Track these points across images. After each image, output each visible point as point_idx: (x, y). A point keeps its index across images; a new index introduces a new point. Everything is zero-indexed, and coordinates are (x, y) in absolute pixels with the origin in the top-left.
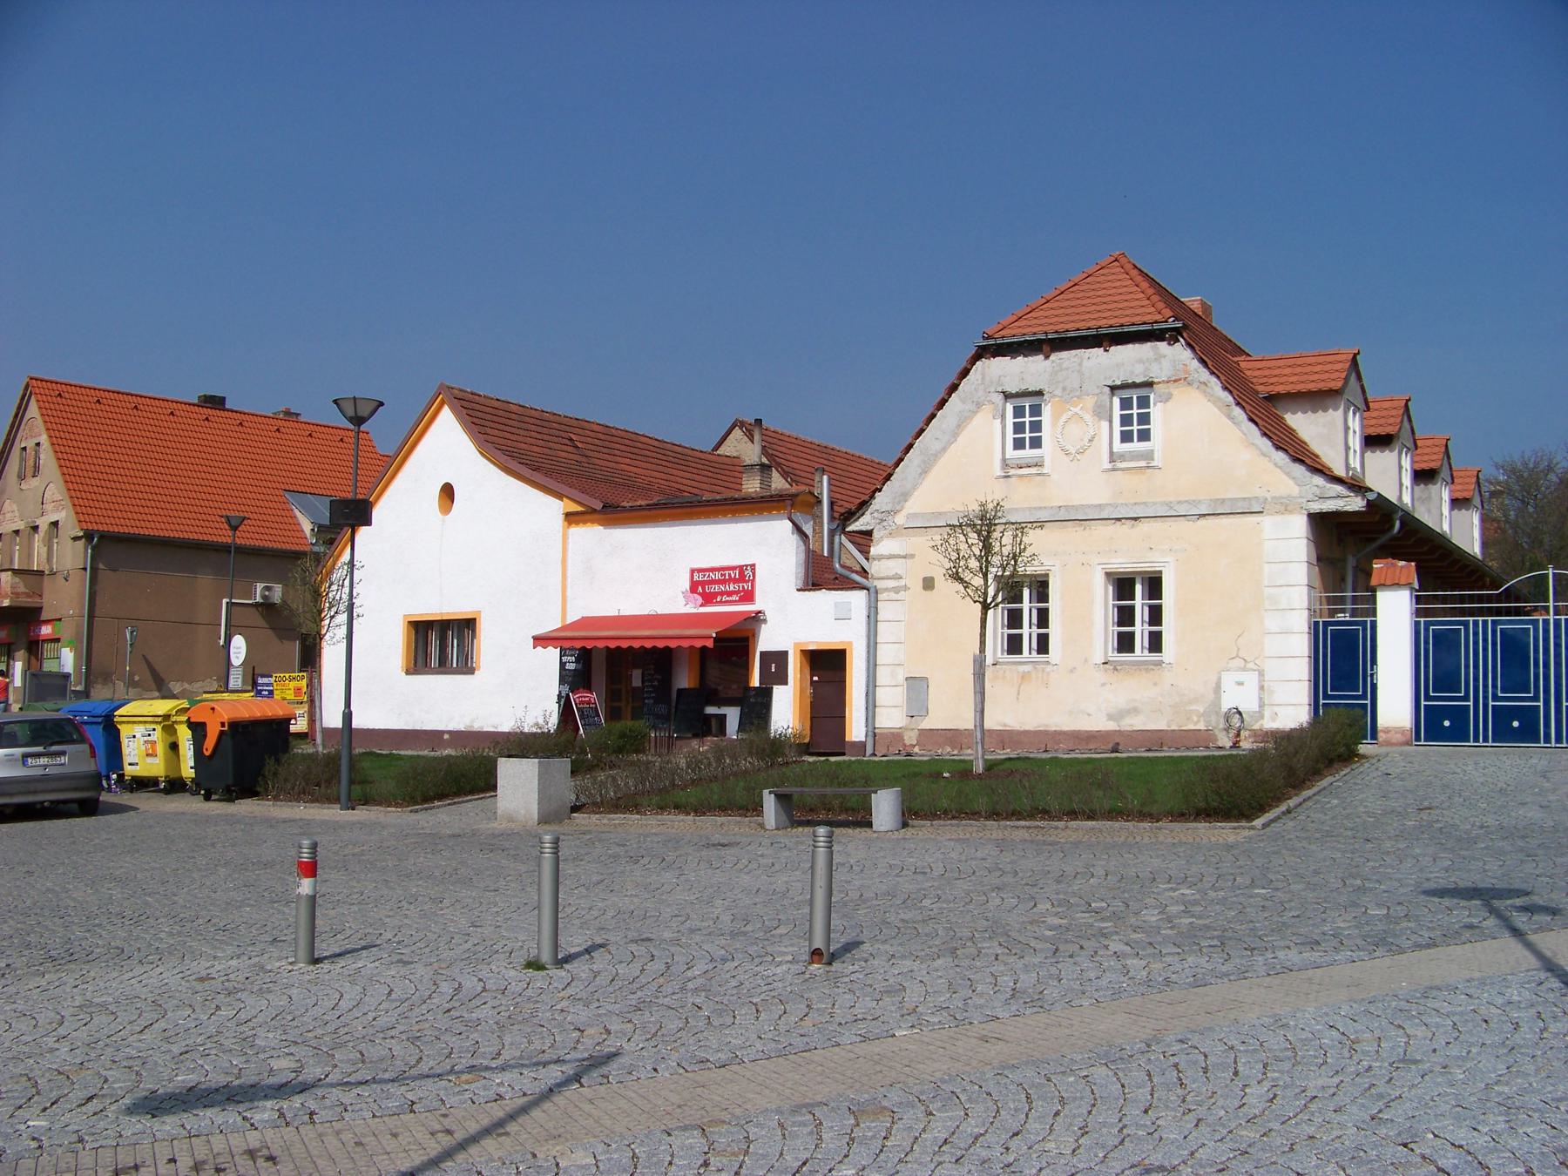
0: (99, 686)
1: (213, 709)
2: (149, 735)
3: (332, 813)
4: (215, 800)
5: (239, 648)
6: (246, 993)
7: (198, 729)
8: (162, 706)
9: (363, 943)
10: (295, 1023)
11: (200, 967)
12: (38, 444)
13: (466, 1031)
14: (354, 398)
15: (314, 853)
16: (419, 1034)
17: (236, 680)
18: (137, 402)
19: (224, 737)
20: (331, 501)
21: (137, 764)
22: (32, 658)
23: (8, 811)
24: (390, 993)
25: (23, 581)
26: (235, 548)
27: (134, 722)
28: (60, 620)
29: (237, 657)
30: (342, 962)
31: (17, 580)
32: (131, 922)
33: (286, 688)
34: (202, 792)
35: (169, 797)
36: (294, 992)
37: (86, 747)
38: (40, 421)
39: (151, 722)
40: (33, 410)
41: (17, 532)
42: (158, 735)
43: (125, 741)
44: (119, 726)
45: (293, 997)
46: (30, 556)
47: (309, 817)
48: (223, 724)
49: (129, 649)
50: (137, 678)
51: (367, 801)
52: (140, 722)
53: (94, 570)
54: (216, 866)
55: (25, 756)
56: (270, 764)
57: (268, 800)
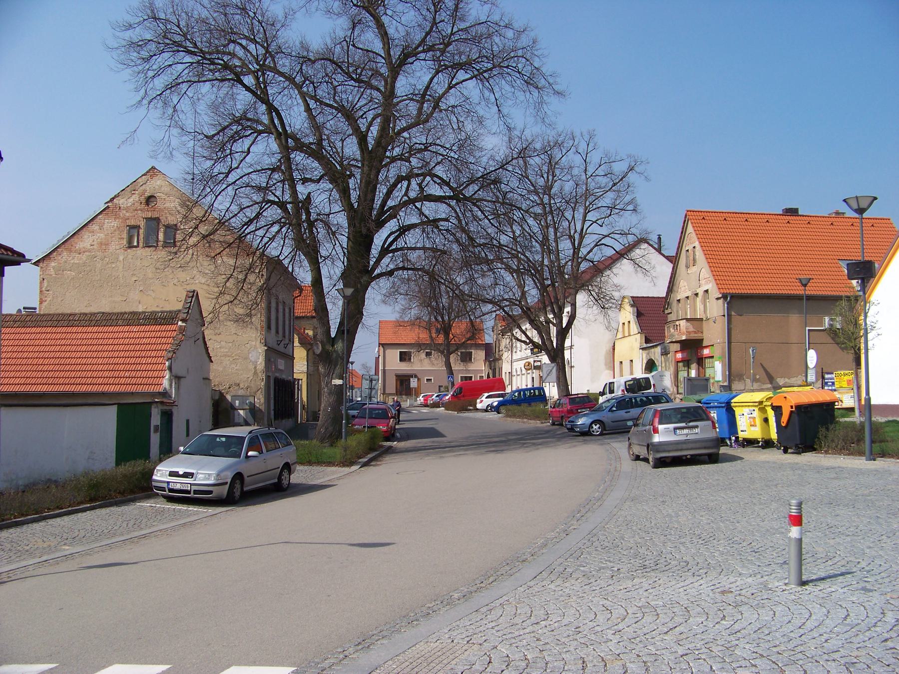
0: (737, 382)
1: (785, 398)
2: (752, 414)
3: (859, 463)
4: (790, 453)
5: (812, 357)
6: (747, 607)
7: (777, 410)
8: (758, 396)
9: (843, 570)
10: (768, 638)
11: (725, 582)
12: (694, 247)
13: (895, 664)
14: (857, 197)
15: (800, 509)
16: (855, 660)
17: (811, 377)
18: (746, 217)
19: (793, 414)
20: (848, 264)
21: (745, 431)
22: (700, 368)
23: (668, 460)
24: (845, 619)
25: (692, 325)
26: (806, 297)
27: (743, 406)
28: (713, 345)
29: (812, 363)
30: (822, 585)
31: (689, 324)
32: (703, 542)
33: (842, 378)
34: (782, 448)
35: (765, 451)
36: (779, 609)
37: (709, 423)
38: (694, 235)
39: (752, 406)
40: (690, 229)
41: (687, 297)
42: (756, 414)
43: (738, 418)
44: (734, 409)
45: (776, 613)
46: (695, 310)
47: (844, 466)
48: (792, 407)
49: (752, 360)
50: (758, 377)
51: (883, 454)
52: (746, 406)
53: (729, 316)
54: (772, 501)
55: (675, 429)
56: (822, 431)
57: (822, 453)
